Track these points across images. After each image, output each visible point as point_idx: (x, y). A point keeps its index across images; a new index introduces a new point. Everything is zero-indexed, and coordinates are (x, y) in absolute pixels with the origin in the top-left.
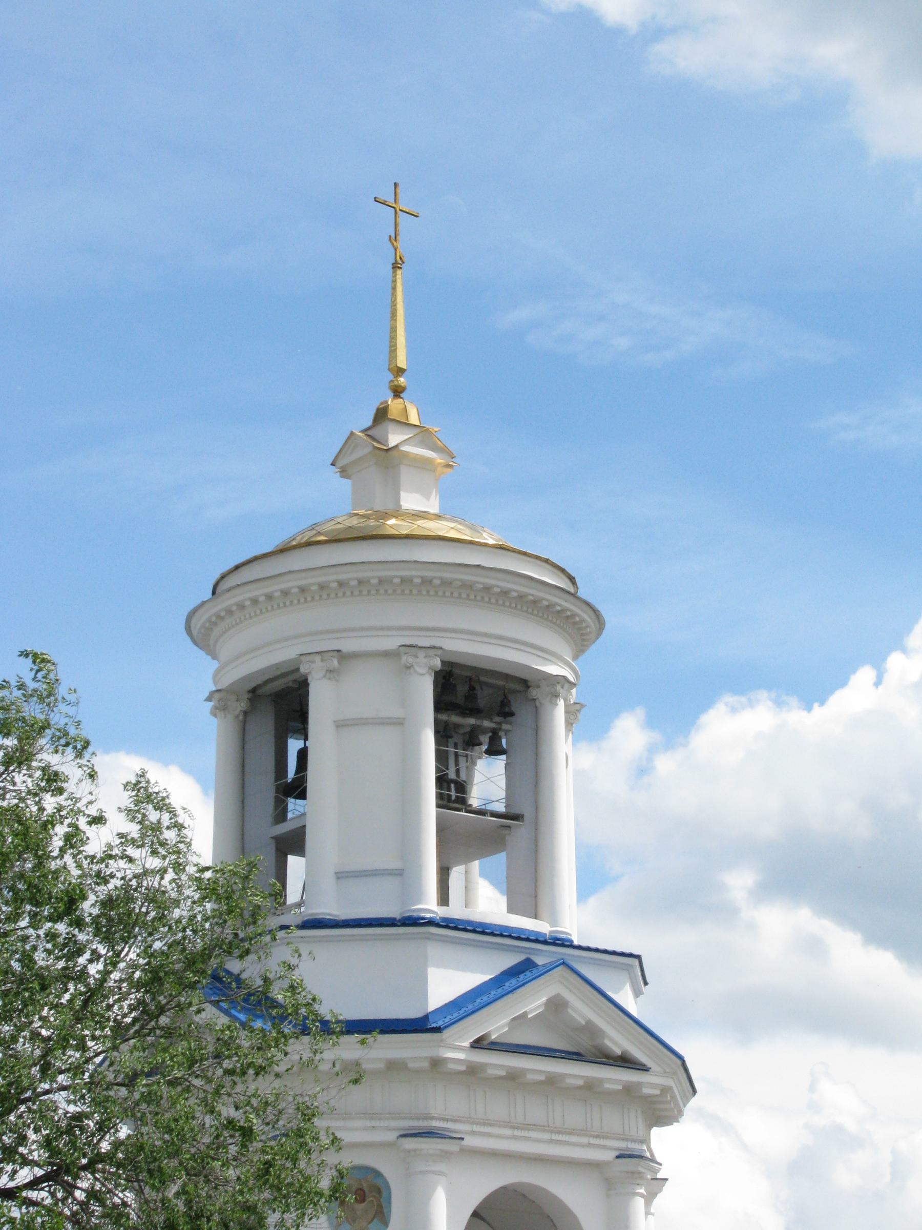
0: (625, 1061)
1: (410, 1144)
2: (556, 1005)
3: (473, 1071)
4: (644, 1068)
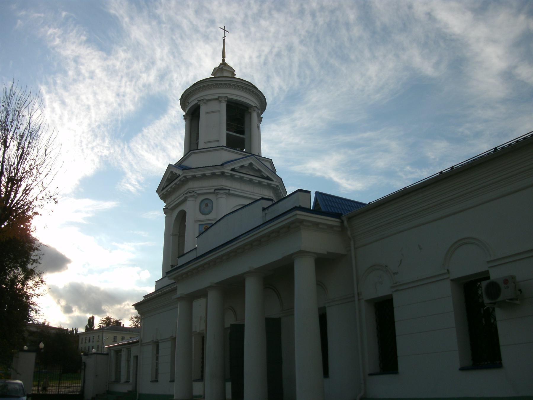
0: (268, 178)
1: (217, 191)
2: (251, 164)
3: (232, 176)
4: (273, 181)
